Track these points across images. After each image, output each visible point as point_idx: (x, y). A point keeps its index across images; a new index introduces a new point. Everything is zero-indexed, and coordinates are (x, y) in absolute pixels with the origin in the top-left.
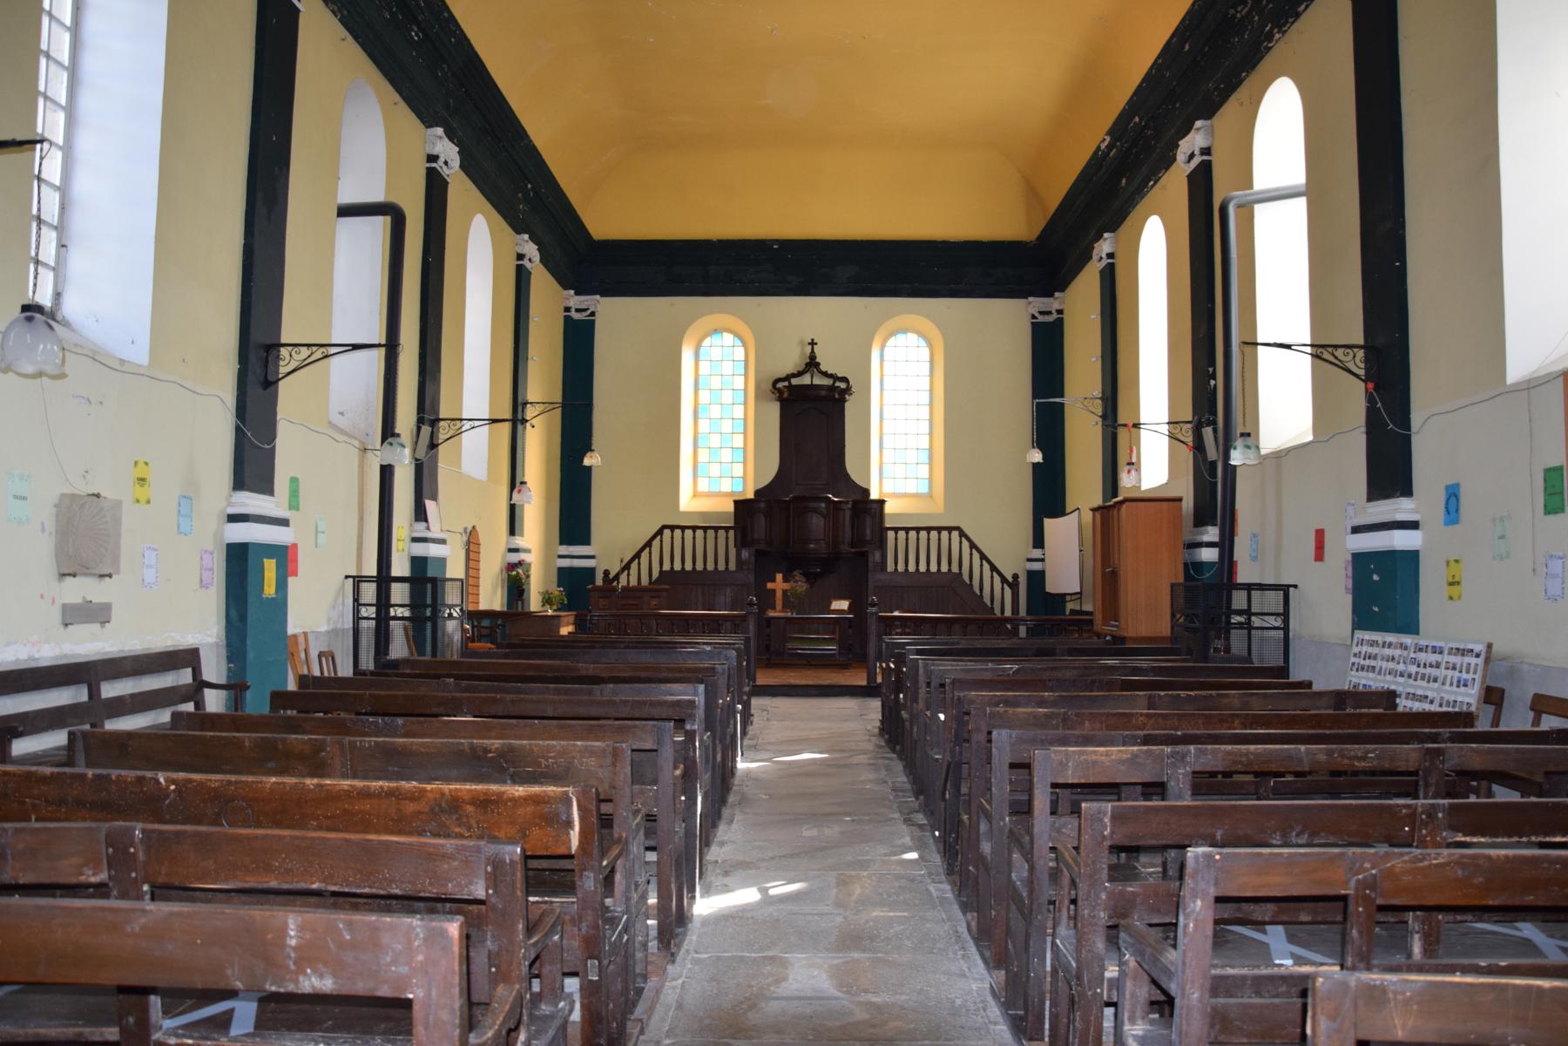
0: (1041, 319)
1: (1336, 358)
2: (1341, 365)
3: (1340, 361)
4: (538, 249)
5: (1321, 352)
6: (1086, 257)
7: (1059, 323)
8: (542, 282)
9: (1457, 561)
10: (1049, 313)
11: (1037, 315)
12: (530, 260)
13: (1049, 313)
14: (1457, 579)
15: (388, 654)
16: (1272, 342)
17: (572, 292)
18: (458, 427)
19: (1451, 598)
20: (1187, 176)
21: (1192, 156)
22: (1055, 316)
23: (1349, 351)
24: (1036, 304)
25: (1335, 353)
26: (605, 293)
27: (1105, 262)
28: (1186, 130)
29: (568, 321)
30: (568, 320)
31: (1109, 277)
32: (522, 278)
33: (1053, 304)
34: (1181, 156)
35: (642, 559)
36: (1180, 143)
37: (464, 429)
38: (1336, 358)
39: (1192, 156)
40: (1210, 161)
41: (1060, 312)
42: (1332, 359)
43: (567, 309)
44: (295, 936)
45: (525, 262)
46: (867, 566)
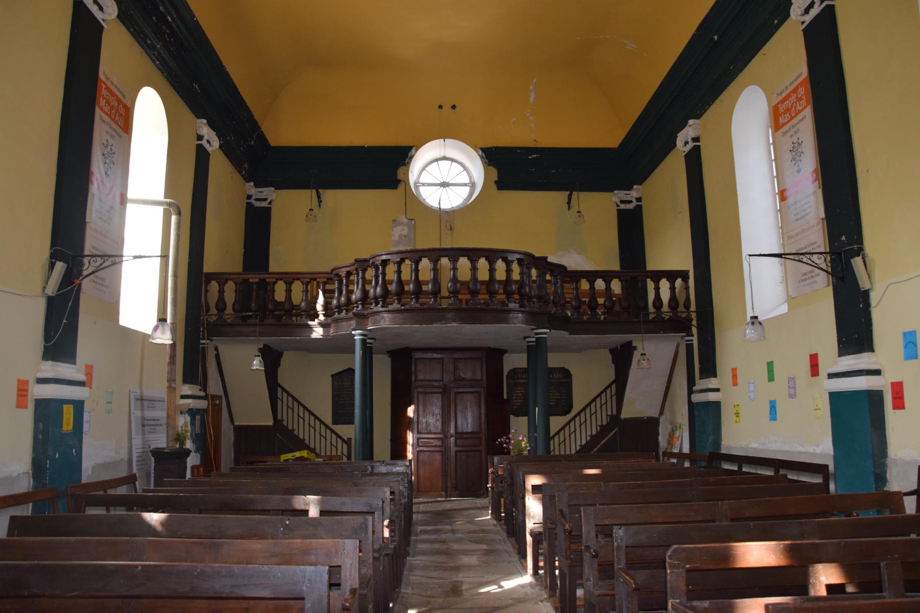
0: (623, 206)
1: (813, 262)
2: (816, 266)
3: (816, 264)
4: (216, 135)
5: (802, 258)
6: (671, 145)
7: (639, 209)
8: (220, 167)
9: (738, 405)
10: (630, 202)
11: (619, 203)
12: (208, 142)
13: (630, 202)
14: (738, 412)
15: (185, 445)
16: (759, 254)
17: (252, 184)
18: (98, 263)
19: (736, 422)
20: (803, 30)
21: (686, 143)
22: (635, 204)
23: (820, 256)
24: (620, 195)
25: (811, 258)
26: (279, 186)
27: (691, 145)
28: (683, 125)
29: (250, 208)
30: (249, 205)
31: (694, 160)
32: (202, 156)
33: (634, 194)
34: (679, 143)
35: (602, 397)
36: (678, 135)
37: (104, 265)
38: (813, 262)
39: (686, 143)
40: (699, 146)
41: (639, 200)
42: (810, 262)
43: (249, 197)
44: (604, 305)
45: (204, 143)
46: (614, 572)
